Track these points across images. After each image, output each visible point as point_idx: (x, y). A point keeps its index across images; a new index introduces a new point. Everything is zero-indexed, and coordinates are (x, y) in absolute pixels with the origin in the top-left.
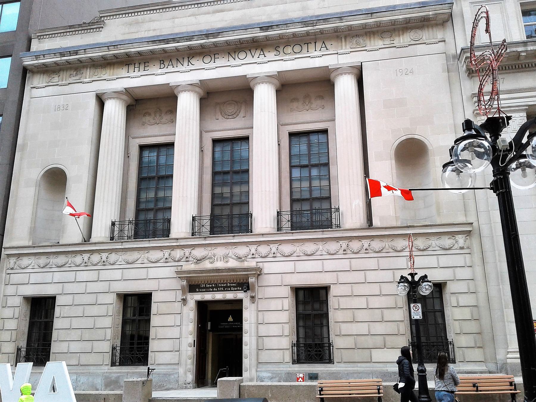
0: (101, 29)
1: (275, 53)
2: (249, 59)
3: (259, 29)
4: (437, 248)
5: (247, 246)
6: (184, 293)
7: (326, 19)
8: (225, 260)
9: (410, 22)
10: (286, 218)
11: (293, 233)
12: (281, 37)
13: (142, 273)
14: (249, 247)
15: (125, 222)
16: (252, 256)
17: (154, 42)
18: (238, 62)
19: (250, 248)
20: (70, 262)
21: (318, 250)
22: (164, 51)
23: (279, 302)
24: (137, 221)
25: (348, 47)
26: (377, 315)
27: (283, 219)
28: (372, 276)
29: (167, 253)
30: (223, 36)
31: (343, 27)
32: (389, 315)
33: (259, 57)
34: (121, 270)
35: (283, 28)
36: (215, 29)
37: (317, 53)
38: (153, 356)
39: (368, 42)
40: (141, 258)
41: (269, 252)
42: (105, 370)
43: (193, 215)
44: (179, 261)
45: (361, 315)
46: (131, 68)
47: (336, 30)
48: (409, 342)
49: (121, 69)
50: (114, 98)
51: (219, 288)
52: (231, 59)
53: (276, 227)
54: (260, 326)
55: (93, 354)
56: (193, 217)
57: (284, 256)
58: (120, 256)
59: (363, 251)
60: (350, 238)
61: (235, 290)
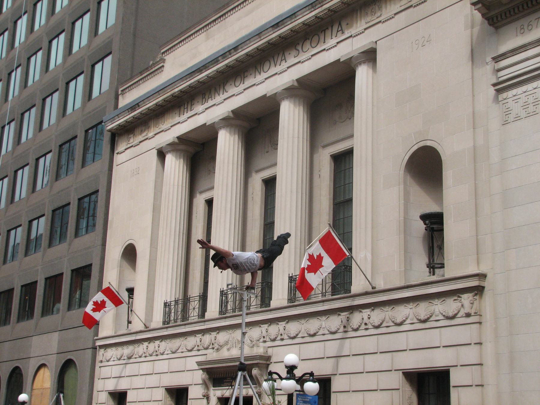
3: (271, 29)
4: (441, 317)
6: (207, 388)
21: (320, 328)
40: (182, 345)
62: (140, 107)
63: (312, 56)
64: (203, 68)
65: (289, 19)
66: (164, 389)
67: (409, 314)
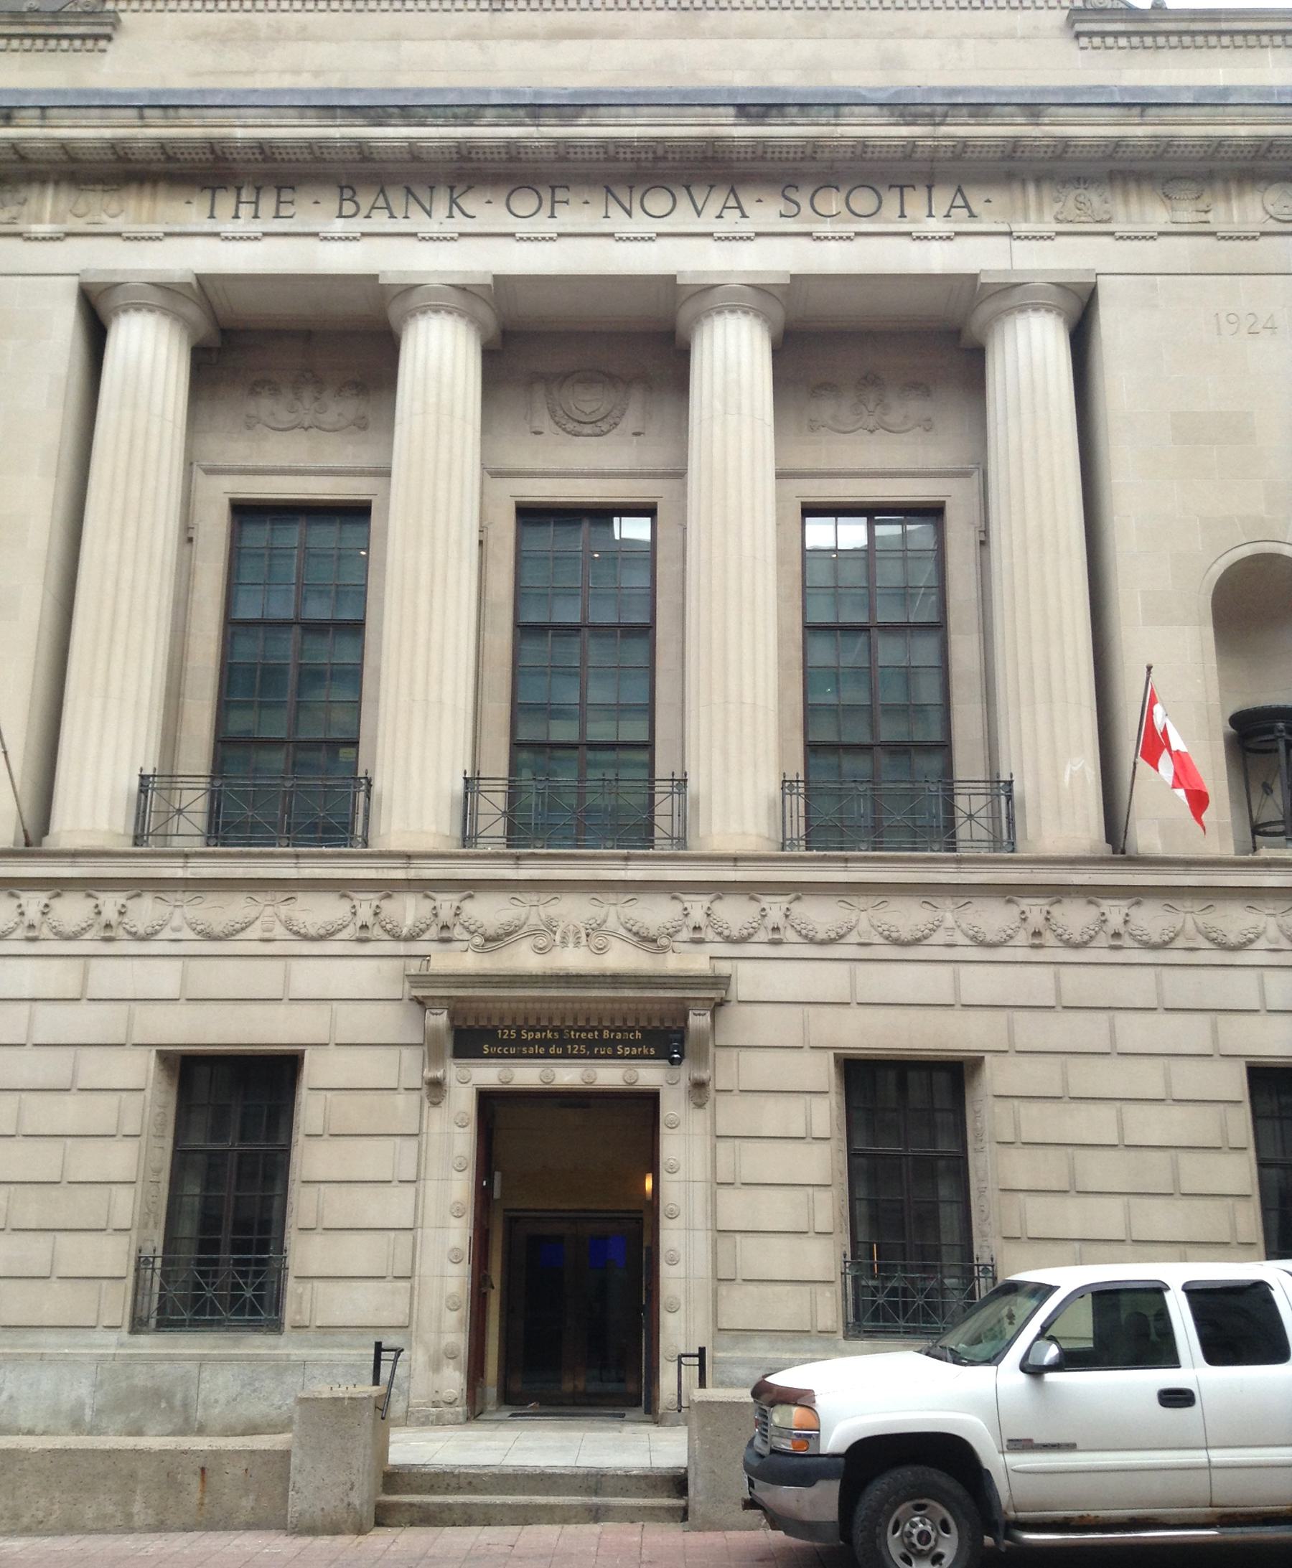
0: (102, 44)
1: (781, 205)
2: (684, 218)
3: (732, 111)
5: (674, 898)
6: (433, 1055)
7: (980, 110)
8: (597, 941)
9: (1064, 155)
10: (494, 802)
11: (518, 858)
12: (813, 149)
13: (264, 978)
14: (682, 902)
15: (174, 779)
16: (770, 937)
17: (330, 112)
18: (640, 224)
19: (687, 905)
20: (176, 921)
22: (363, 151)
23: (795, 1107)
24: (514, 781)
25: (1048, 217)
26: (1156, 1171)
27: (483, 805)
28: (1135, 1032)
29: (366, 904)
30: (596, 121)
31: (1037, 143)
32: (1198, 1173)
33: (948, 216)
34: (178, 964)
35: (824, 120)
36: (567, 92)
37: (936, 225)
38: (306, 1297)
39: (1119, 209)
41: (755, 925)
42: (106, 1346)
43: (141, 770)
44: (412, 938)
45: (1098, 1171)
46: (226, 202)
47: (1013, 148)
48: (845, 1262)
49: (182, 203)
50: (151, 309)
51: (569, 1047)
52: (616, 212)
53: (458, 833)
54: (723, 1193)
55: (55, 1285)
56: (142, 777)
57: (812, 941)
58: (175, 906)
59: (1103, 940)
60: (1058, 892)
61: (630, 1057)
62: (47, 122)
63: (858, 234)
64: (396, 111)
65: (346, 112)
66: (154, 1053)
67: (858, 920)
